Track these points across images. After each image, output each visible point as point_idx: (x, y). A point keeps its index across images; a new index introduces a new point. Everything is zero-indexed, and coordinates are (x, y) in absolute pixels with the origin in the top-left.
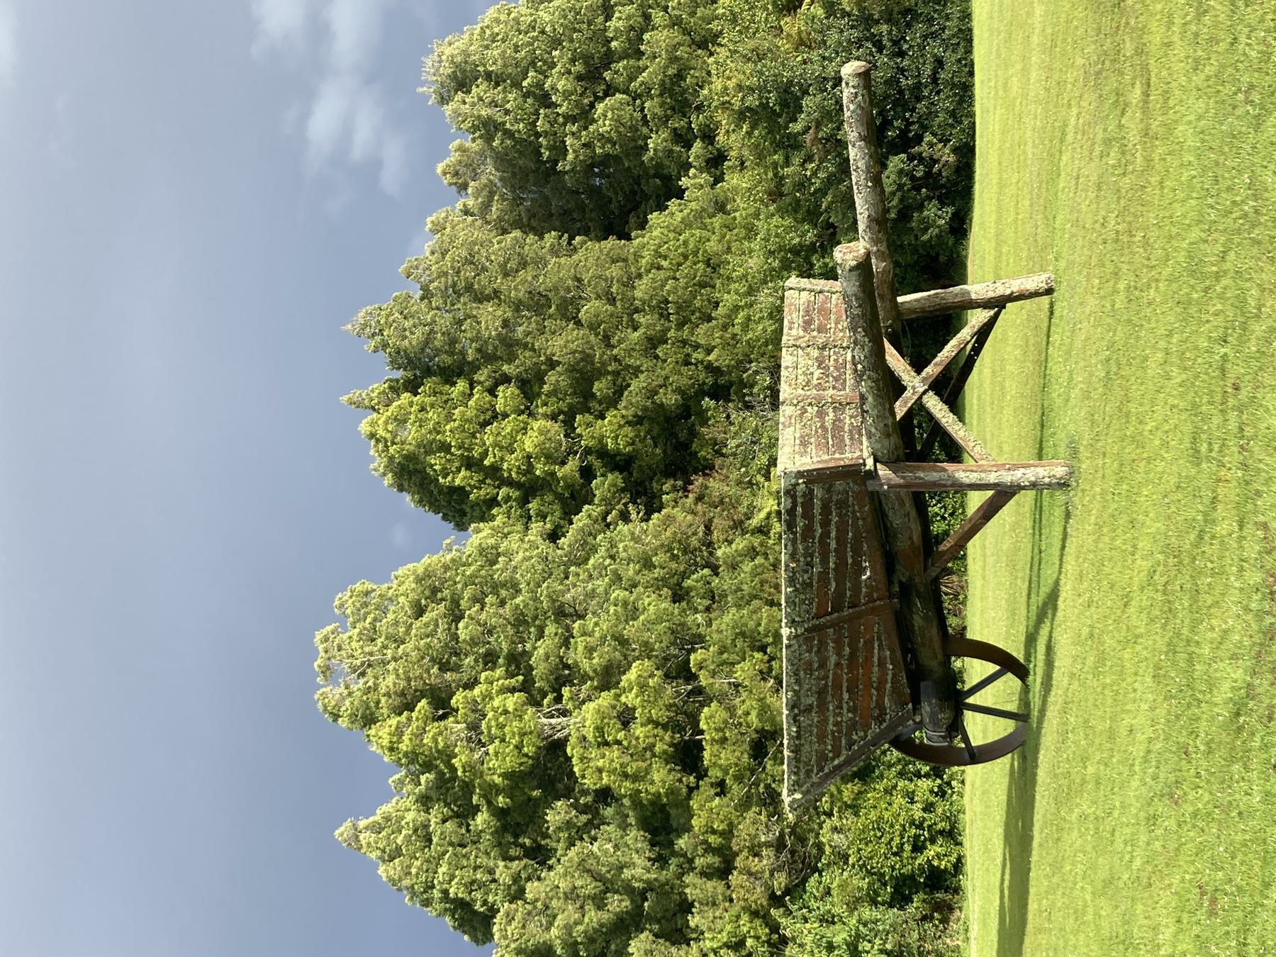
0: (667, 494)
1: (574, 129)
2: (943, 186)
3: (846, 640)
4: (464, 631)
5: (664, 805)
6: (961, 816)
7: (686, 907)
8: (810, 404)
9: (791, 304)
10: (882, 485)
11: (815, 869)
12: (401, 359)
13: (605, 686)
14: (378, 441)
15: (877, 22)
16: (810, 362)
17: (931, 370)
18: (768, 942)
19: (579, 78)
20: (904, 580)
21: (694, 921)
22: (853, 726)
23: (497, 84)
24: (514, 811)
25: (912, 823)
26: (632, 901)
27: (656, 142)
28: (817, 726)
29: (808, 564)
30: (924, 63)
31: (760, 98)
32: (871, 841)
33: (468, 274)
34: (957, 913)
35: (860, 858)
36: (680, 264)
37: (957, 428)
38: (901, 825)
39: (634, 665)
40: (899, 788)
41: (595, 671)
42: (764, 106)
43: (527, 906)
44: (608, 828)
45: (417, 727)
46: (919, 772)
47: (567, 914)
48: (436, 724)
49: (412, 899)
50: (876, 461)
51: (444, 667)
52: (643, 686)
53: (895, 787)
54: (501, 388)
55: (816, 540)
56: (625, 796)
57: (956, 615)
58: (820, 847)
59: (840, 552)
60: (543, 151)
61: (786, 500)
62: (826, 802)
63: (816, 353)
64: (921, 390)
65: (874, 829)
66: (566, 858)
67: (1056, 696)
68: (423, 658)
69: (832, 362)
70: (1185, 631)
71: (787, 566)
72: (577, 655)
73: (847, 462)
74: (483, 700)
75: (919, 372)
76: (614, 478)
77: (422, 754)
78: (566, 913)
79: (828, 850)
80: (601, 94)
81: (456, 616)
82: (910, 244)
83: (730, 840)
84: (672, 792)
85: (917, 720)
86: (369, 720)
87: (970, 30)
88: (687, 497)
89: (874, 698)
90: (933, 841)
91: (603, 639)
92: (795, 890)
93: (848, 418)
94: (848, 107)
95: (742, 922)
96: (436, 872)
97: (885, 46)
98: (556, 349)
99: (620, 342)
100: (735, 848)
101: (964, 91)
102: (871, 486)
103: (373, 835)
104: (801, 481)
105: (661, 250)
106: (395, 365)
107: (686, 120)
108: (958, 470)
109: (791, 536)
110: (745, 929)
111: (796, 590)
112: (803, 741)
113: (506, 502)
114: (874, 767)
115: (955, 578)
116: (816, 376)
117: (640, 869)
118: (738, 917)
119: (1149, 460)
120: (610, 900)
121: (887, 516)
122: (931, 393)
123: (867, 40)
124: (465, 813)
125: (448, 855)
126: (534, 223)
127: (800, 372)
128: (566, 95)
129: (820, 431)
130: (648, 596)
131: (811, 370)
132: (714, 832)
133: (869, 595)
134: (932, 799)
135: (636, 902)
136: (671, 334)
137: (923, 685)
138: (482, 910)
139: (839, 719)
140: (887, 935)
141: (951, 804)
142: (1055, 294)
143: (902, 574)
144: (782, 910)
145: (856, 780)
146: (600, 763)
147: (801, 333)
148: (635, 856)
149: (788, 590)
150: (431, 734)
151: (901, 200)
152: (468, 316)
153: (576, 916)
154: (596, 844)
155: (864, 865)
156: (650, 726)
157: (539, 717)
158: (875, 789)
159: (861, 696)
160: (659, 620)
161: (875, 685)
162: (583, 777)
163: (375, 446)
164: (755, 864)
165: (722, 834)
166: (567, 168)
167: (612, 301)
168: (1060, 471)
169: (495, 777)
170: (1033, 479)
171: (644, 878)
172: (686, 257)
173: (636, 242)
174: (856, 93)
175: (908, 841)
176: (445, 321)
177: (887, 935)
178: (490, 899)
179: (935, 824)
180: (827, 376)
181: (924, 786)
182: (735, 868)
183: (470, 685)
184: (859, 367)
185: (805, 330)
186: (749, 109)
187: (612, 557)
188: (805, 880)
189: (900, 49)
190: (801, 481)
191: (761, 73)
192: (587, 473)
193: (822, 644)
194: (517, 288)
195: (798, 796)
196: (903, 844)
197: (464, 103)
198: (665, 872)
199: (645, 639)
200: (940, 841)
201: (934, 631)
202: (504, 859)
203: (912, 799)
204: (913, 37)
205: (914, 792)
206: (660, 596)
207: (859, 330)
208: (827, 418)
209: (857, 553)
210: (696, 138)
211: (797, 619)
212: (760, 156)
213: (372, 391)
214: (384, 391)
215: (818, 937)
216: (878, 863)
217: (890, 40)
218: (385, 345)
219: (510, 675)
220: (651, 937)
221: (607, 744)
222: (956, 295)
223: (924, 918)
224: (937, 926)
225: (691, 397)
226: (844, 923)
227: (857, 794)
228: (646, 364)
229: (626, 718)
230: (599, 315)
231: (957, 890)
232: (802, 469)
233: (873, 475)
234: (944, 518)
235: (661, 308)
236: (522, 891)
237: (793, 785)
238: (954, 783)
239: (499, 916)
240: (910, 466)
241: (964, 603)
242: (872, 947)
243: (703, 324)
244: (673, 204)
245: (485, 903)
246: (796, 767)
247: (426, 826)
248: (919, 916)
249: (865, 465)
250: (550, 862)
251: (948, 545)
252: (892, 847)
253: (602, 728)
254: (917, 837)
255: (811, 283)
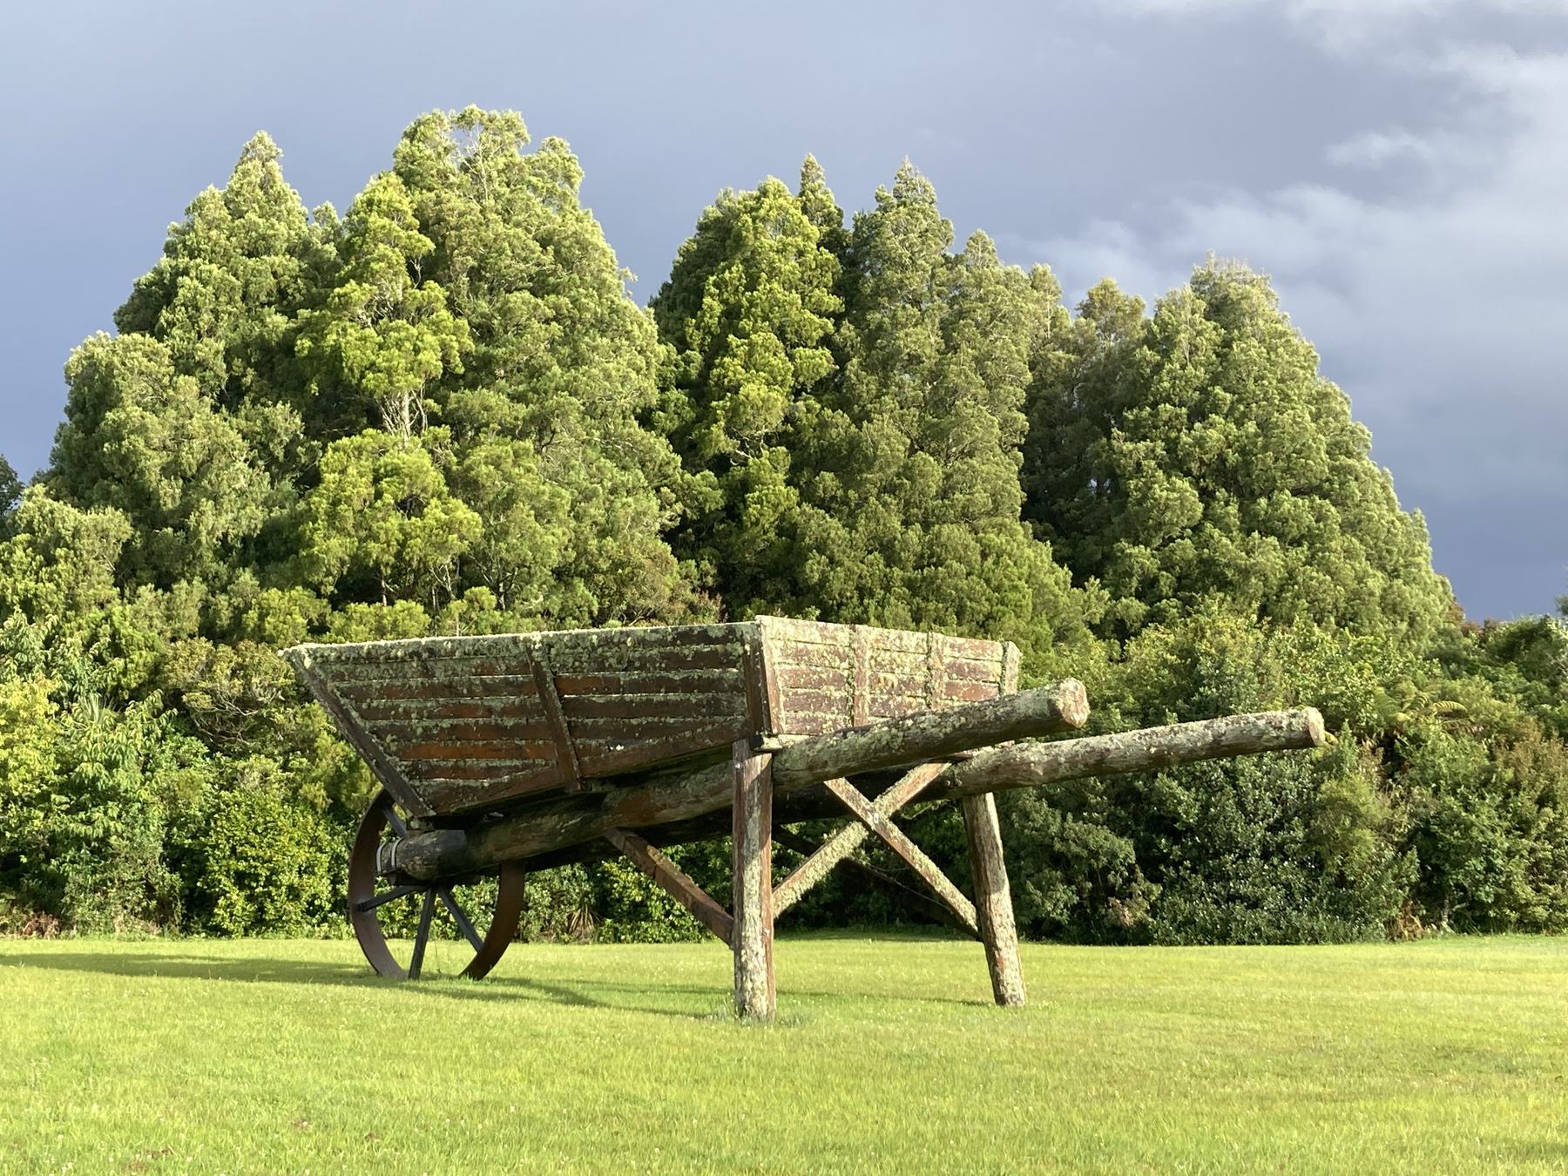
0: (698, 566)
1: (1159, 451)
2: (1095, 910)
3: (524, 721)
4: (520, 299)
5: (297, 553)
6: (283, 935)
7: (164, 582)
8: (852, 666)
9: (984, 650)
10: (742, 761)
11: (213, 749)
12: (869, 229)
13: (450, 479)
14: (758, 198)
15: (1307, 825)
16: (907, 670)
17: (896, 836)
18: (119, 686)
19: (1222, 459)
20: (606, 800)
21: (146, 592)
22: (403, 734)
23: (1218, 355)
24: (290, 363)
25: (273, 872)
26: (172, 512)
27: (1142, 556)
28: (404, 685)
29: (631, 663)
30: (1254, 885)
31: (1211, 677)
32: (250, 819)
33: (979, 311)
34: (157, 931)
35: (228, 806)
36: (988, 581)
37: (819, 866)
38: (271, 857)
39: (476, 515)
40: (319, 855)
41: (470, 468)
42: (1199, 681)
43: (168, 378)
44: (266, 483)
45: (399, 238)
46: (339, 883)
47: (159, 428)
48: (402, 261)
49: (176, 231)
50: (775, 753)
51: (475, 274)
52: (448, 527)
53: (321, 850)
54: (828, 352)
55: (664, 674)
56: (308, 504)
57: (542, 930)
58: (244, 754)
59: (647, 708)
60: (1135, 411)
61: (720, 629)
62: (301, 763)
63: (920, 678)
64: (869, 821)
65: (266, 823)
66: (227, 429)
67: (443, 1001)
68: (485, 246)
69: (908, 700)
70: (552, 1138)
71: (628, 634)
72: (488, 447)
73: (773, 711)
74: (433, 324)
75: (895, 818)
76: (716, 498)
77: (364, 241)
78: (160, 428)
79: (240, 764)
80: (1202, 484)
81: (540, 286)
82: (1020, 868)
83: (251, 638)
84: (314, 562)
85: (412, 823)
86: (409, 179)
87: (1298, 943)
88: (693, 591)
89: (442, 764)
90: (250, 899)
91: (507, 478)
92: (187, 722)
93: (833, 717)
94: (1262, 717)
95: (144, 653)
96: (211, 262)
97: (1275, 834)
98: (877, 424)
99: (885, 504)
100: (242, 645)
101: (1220, 935)
102: (740, 747)
103: (258, 180)
104: (747, 647)
105: (1005, 556)
106: (861, 222)
107: (1170, 594)
108: (762, 864)
109: (670, 638)
110: (135, 657)
111: (594, 649)
112: (383, 667)
113: (683, 359)
114: (346, 824)
115: (591, 927)
116: (889, 676)
117: (212, 522)
118: (152, 648)
119: (796, 1097)
120: (173, 483)
121: (696, 771)
122: (865, 834)
123: (1283, 811)
124: (283, 301)
125: (234, 279)
126: (1040, 404)
127: (895, 655)
128: (1200, 442)
129: (815, 677)
130: (564, 534)
131: (897, 671)
132: (262, 617)
133: (587, 750)
134: (305, 896)
135: (172, 517)
136: (897, 571)
137: (461, 833)
138: (162, 320)
139: (413, 715)
140: (128, 838)
141: (298, 922)
142: (998, 1007)
143: (614, 797)
144: (160, 705)
145: (330, 801)
146: (352, 470)
147: (947, 660)
148: (230, 516)
149: (595, 637)
150: (390, 254)
151: (1077, 857)
152: (923, 313)
153: (156, 440)
154: (245, 466)
155: (219, 810)
156: (401, 537)
157: (410, 394)
158: (317, 824)
159: (446, 746)
160: (535, 548)
161: (461, 763)
162: (336, 450)
163: (751, 196)
164: (222, 669)
165: (260, 628)
166: (1114, 442)
167: (944, 494)
168: (761, 1004)
169: (334, 337)
170: (750, 967)
171: (202, 528)
172: (997, 589)
173: (1017, 526)
174: (1281, 728)
175: (251, 866)
176: (917, 282)
177: (128, 838)
178: (176, 331)
179: (273, 901)
180: (889, 693)
181: (321, 886)
182: (215, 645)
183: (451, 304)
184: (909, 722)
185: (950, 666)
186: (1196, 661)
187: (613, 491)
188: (201, 737)
189: (1272, 854)
190: (747, 647)
191: (1241, 678)
192: (721, 464)
193: (517, 688)
194: (960, 368)
195: (308, 663)
196: (246, 860)
197: (1193, 312)
198: (210, 554)
199: (512, 530)
200: (251, 908)
201: (534, 846)
202: (227, 351)
203: (305, 872)
204: (1288, 870)
205: (314, 874)
206: (566, 549)
207: (963, 719)
208: (832, 688)
209: (648, 730)
210: (1151, 605)
211: (553, 651)
212: (1130, 681)
213: (825, 193)
214: (825, 207)
215: (123, 748)
216: (222, 827)
217: (1284, 842)
218: (885, 210)
219: (465, 356)
220: (125, 537)
221: (376, 480)
222: (996, 874)
223: (149, 889)
224: (139, 904)
225: (817, 596)
226: (143, 784)
227: (311, 803)
228: (860, 537)
229: (411, 506)
230: (923, 477)
231: (186, 930)
232: (764, 648)
233: (756, 748)
234: (667, 914)
235: (930, 558)
236: (188, 372)
237: (322, 656)
238: (325, 926)
239: (153, 340)
240: (768, 799)
241: (559, 940)
242: (112, 819)
243: (910, 610)
244: (1065, 574)
245: (171, 324)
246: (348, 658)
247: (268, 251)
248: (153, 880)
249: (769, 736)
250: (224, 409)
251: (655, 858)
252: (242, 845)
253: (398, 474)
254: (256, 877)
255: (1013, 677)
